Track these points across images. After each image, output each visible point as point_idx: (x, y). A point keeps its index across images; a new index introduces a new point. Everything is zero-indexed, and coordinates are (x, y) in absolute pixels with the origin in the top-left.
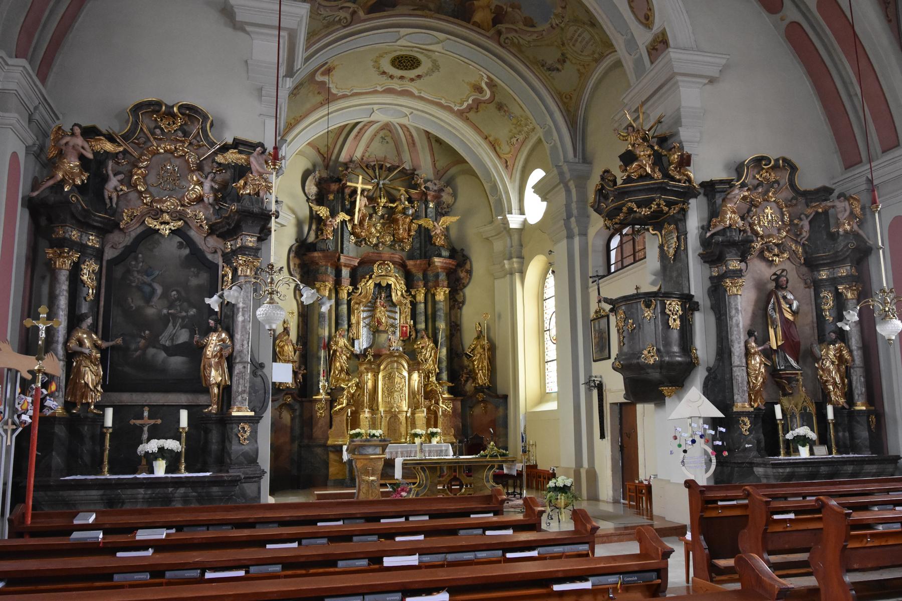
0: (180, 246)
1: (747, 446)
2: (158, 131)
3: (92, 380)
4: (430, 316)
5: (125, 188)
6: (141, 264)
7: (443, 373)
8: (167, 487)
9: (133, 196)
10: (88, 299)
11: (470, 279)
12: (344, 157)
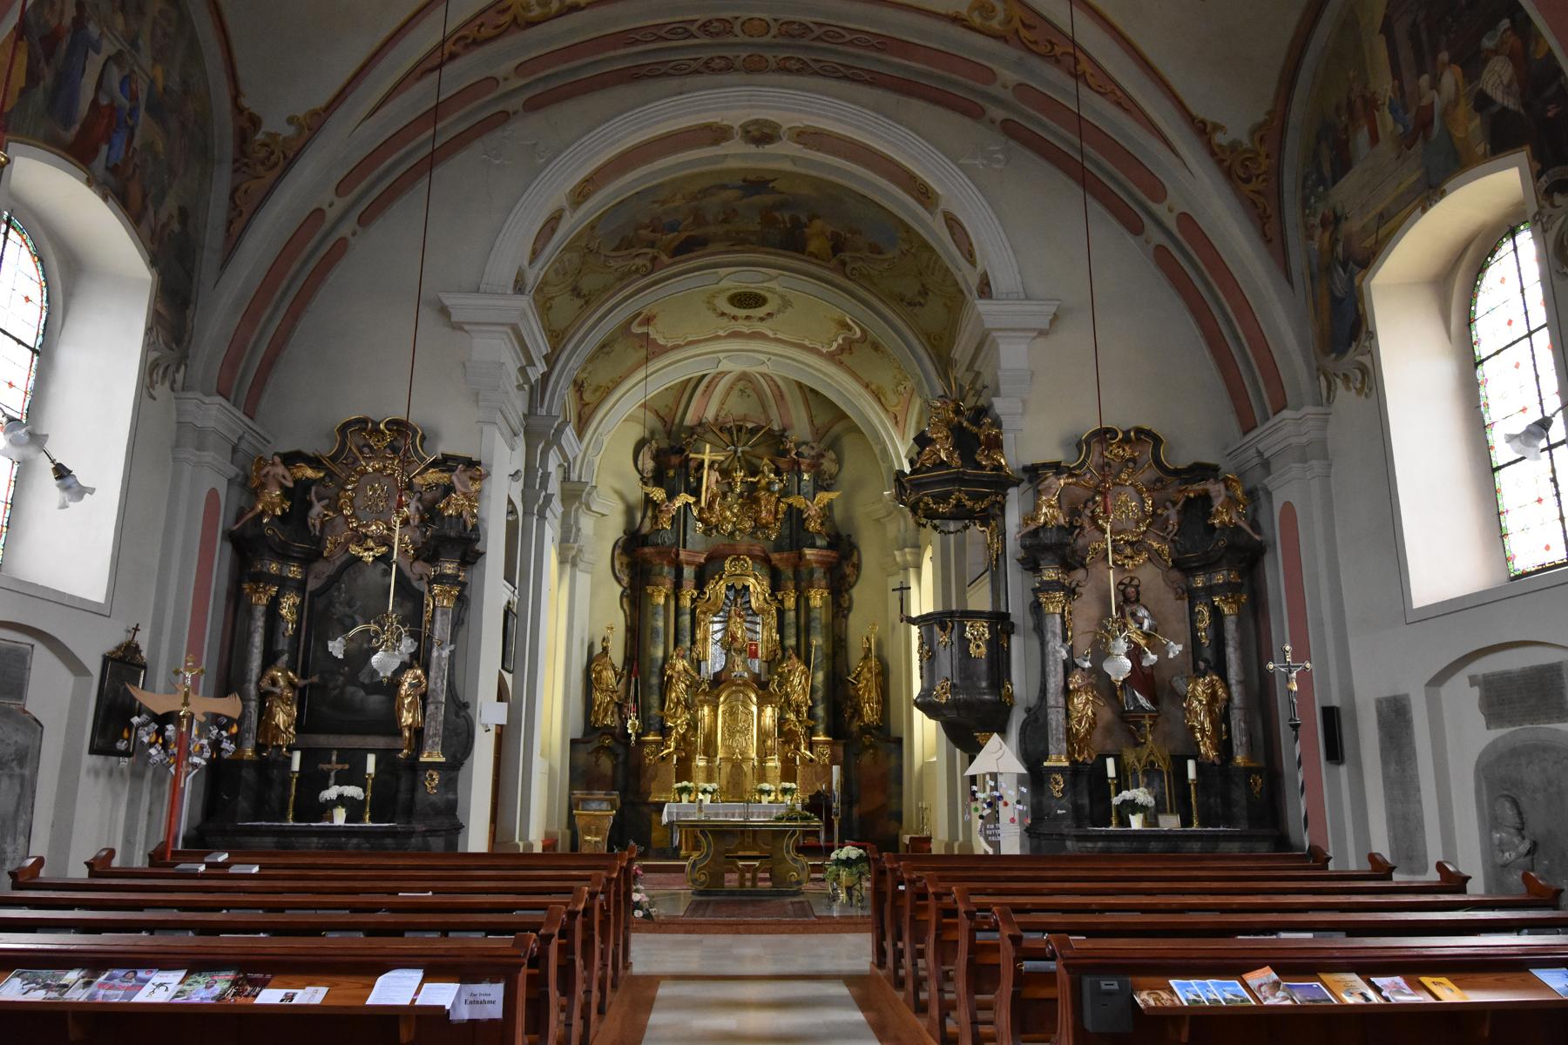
1: (1059, 812)
2: (366, 450)
3: (284, 721)
4: (803, 629)
5: (331, 514)
8: (340, 837)
9: (340, 520)
10: (287, 634)
11: (858, 577)
12: (690, 420)
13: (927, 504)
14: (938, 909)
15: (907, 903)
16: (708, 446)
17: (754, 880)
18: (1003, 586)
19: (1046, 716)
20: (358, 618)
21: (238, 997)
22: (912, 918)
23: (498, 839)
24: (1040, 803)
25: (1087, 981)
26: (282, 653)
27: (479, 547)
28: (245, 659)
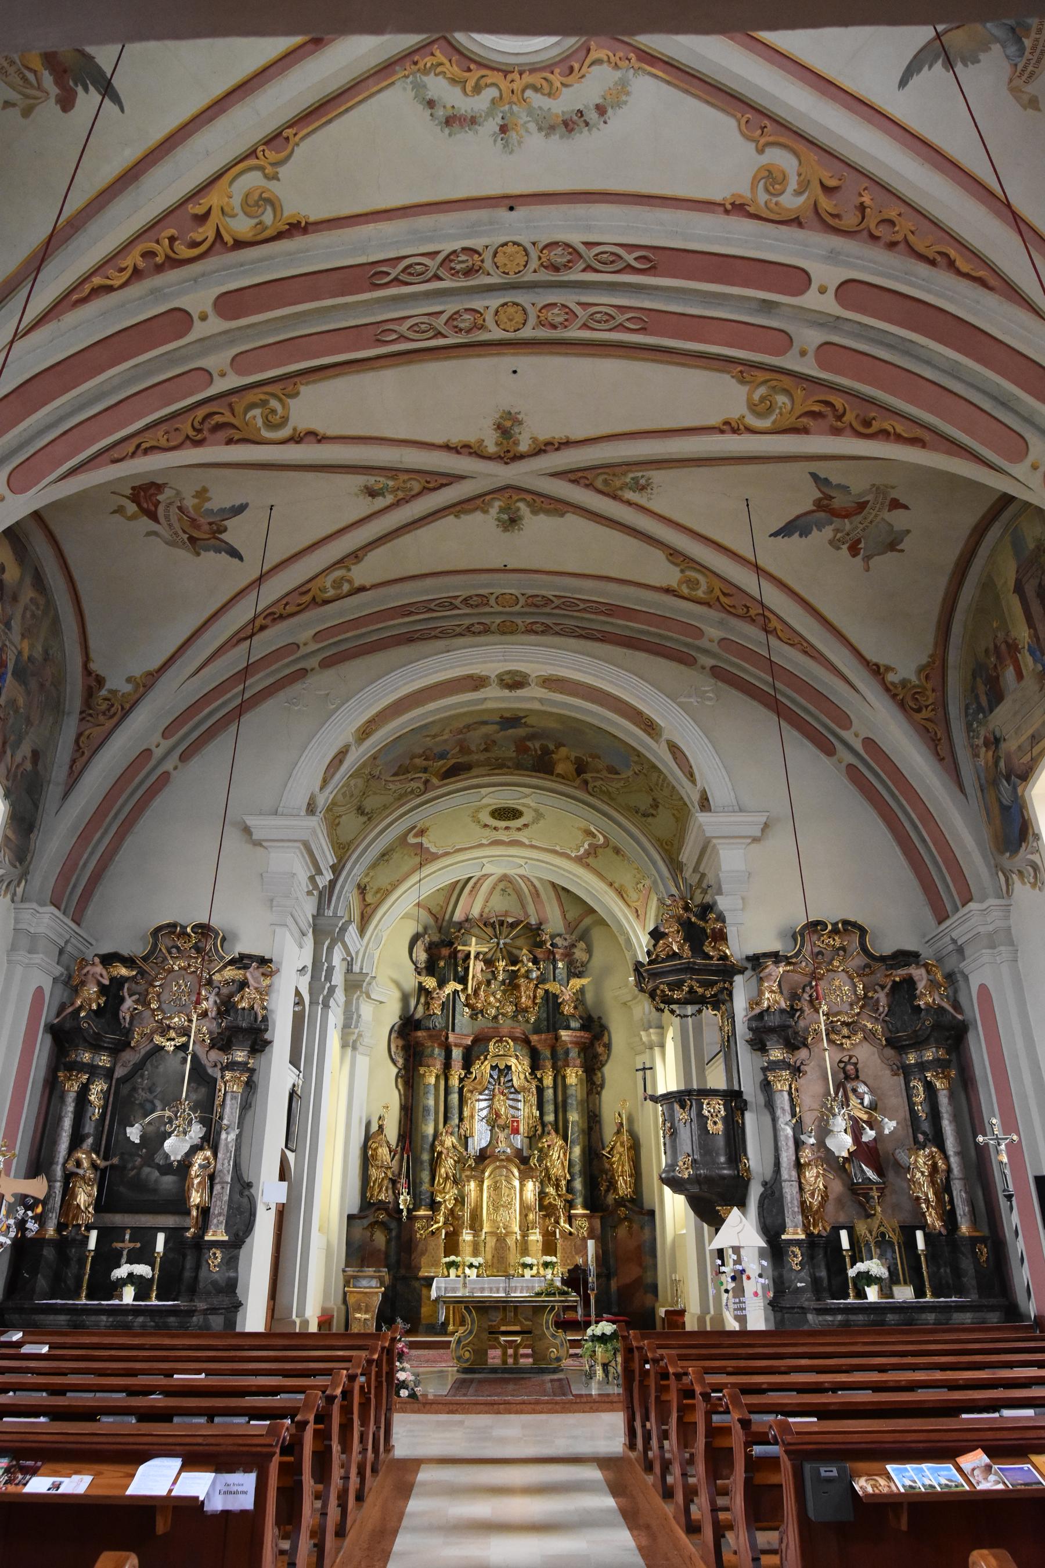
1: (799, 1285)
2: (174, 950)
4: (560, 1105)
5: (140, 1007)
11: (609, 1056)
12: (458, 916)
13: (663, 991)
14: (679, 1390)
15: (652, 1383)
16: (474, 939)
17: (516, 1356)
18: (735, 1064)
19: (781, 1189)
20: (157, 1103)
21: (9, 1486)
22: (657, 1398)
23: (275, 1316)
24: (781, 1276)
25: (807, 1467)
26: (88, 1136)
27: (267, 1036)
28: (54, 1142)
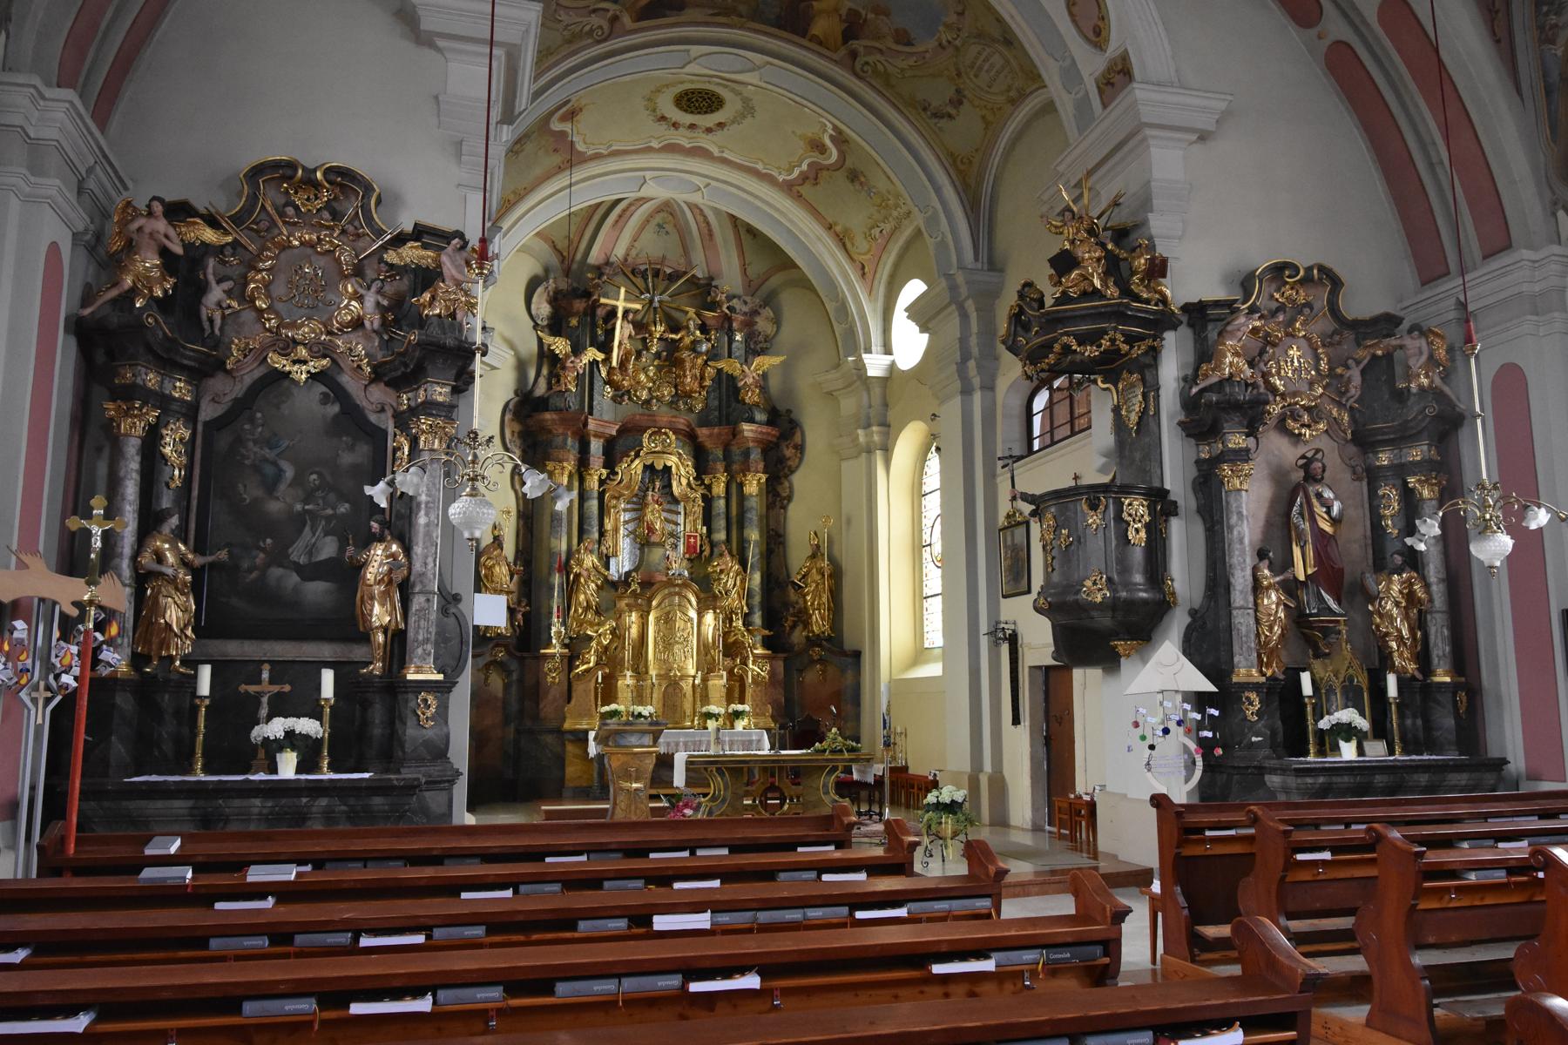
0: (325, 400)
1: (1254, 739)
2: (290, 211)
4: (734, 520)
5: (235, 304)
6: (260, 429)
7: (755, 613)
9: (248, 316)
10: (173, 486)
11: (801, 460)
12: (595, 257)
